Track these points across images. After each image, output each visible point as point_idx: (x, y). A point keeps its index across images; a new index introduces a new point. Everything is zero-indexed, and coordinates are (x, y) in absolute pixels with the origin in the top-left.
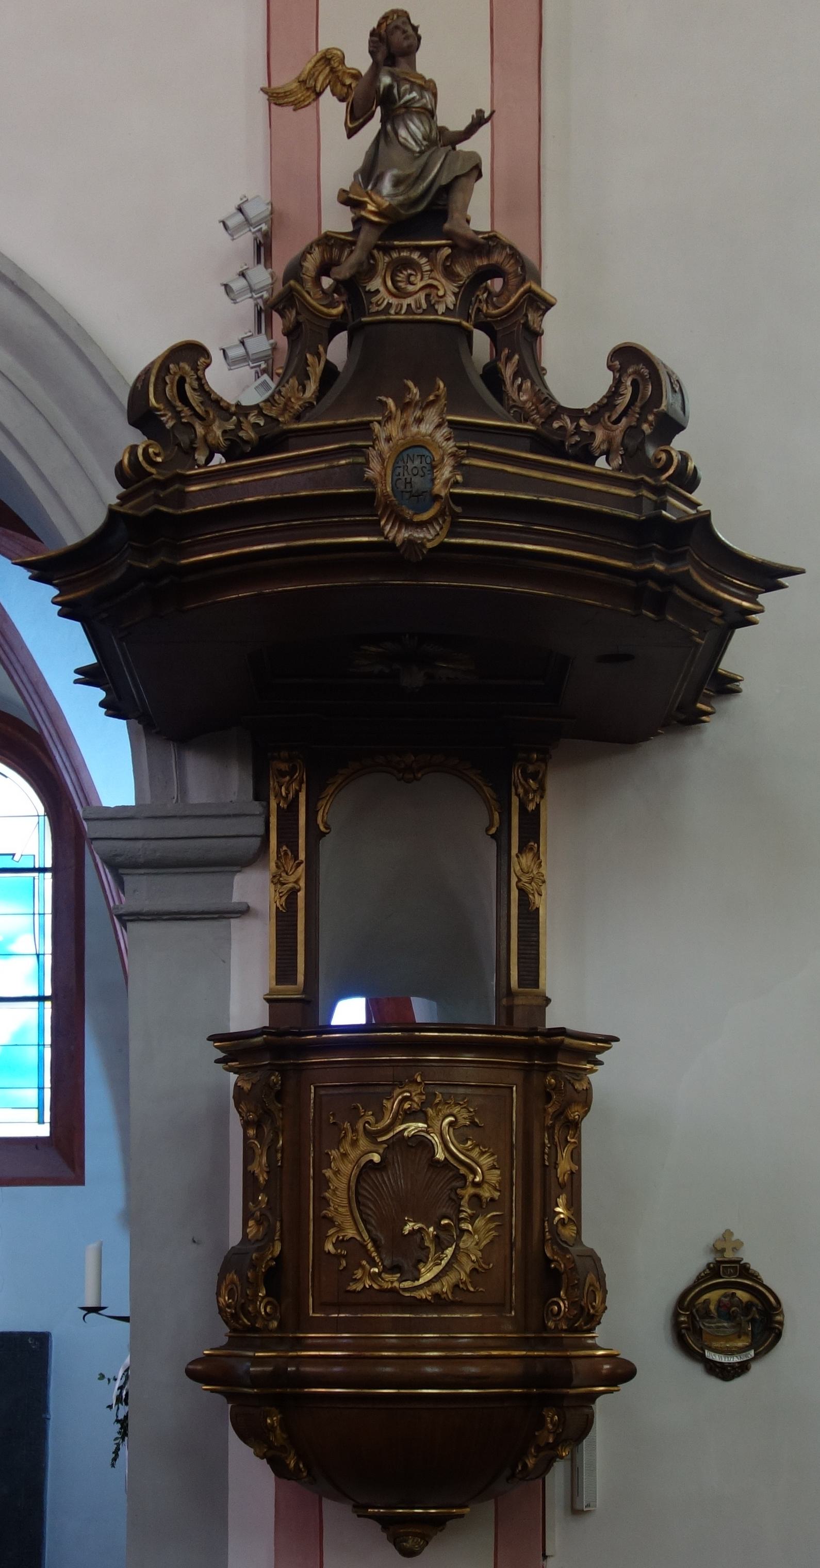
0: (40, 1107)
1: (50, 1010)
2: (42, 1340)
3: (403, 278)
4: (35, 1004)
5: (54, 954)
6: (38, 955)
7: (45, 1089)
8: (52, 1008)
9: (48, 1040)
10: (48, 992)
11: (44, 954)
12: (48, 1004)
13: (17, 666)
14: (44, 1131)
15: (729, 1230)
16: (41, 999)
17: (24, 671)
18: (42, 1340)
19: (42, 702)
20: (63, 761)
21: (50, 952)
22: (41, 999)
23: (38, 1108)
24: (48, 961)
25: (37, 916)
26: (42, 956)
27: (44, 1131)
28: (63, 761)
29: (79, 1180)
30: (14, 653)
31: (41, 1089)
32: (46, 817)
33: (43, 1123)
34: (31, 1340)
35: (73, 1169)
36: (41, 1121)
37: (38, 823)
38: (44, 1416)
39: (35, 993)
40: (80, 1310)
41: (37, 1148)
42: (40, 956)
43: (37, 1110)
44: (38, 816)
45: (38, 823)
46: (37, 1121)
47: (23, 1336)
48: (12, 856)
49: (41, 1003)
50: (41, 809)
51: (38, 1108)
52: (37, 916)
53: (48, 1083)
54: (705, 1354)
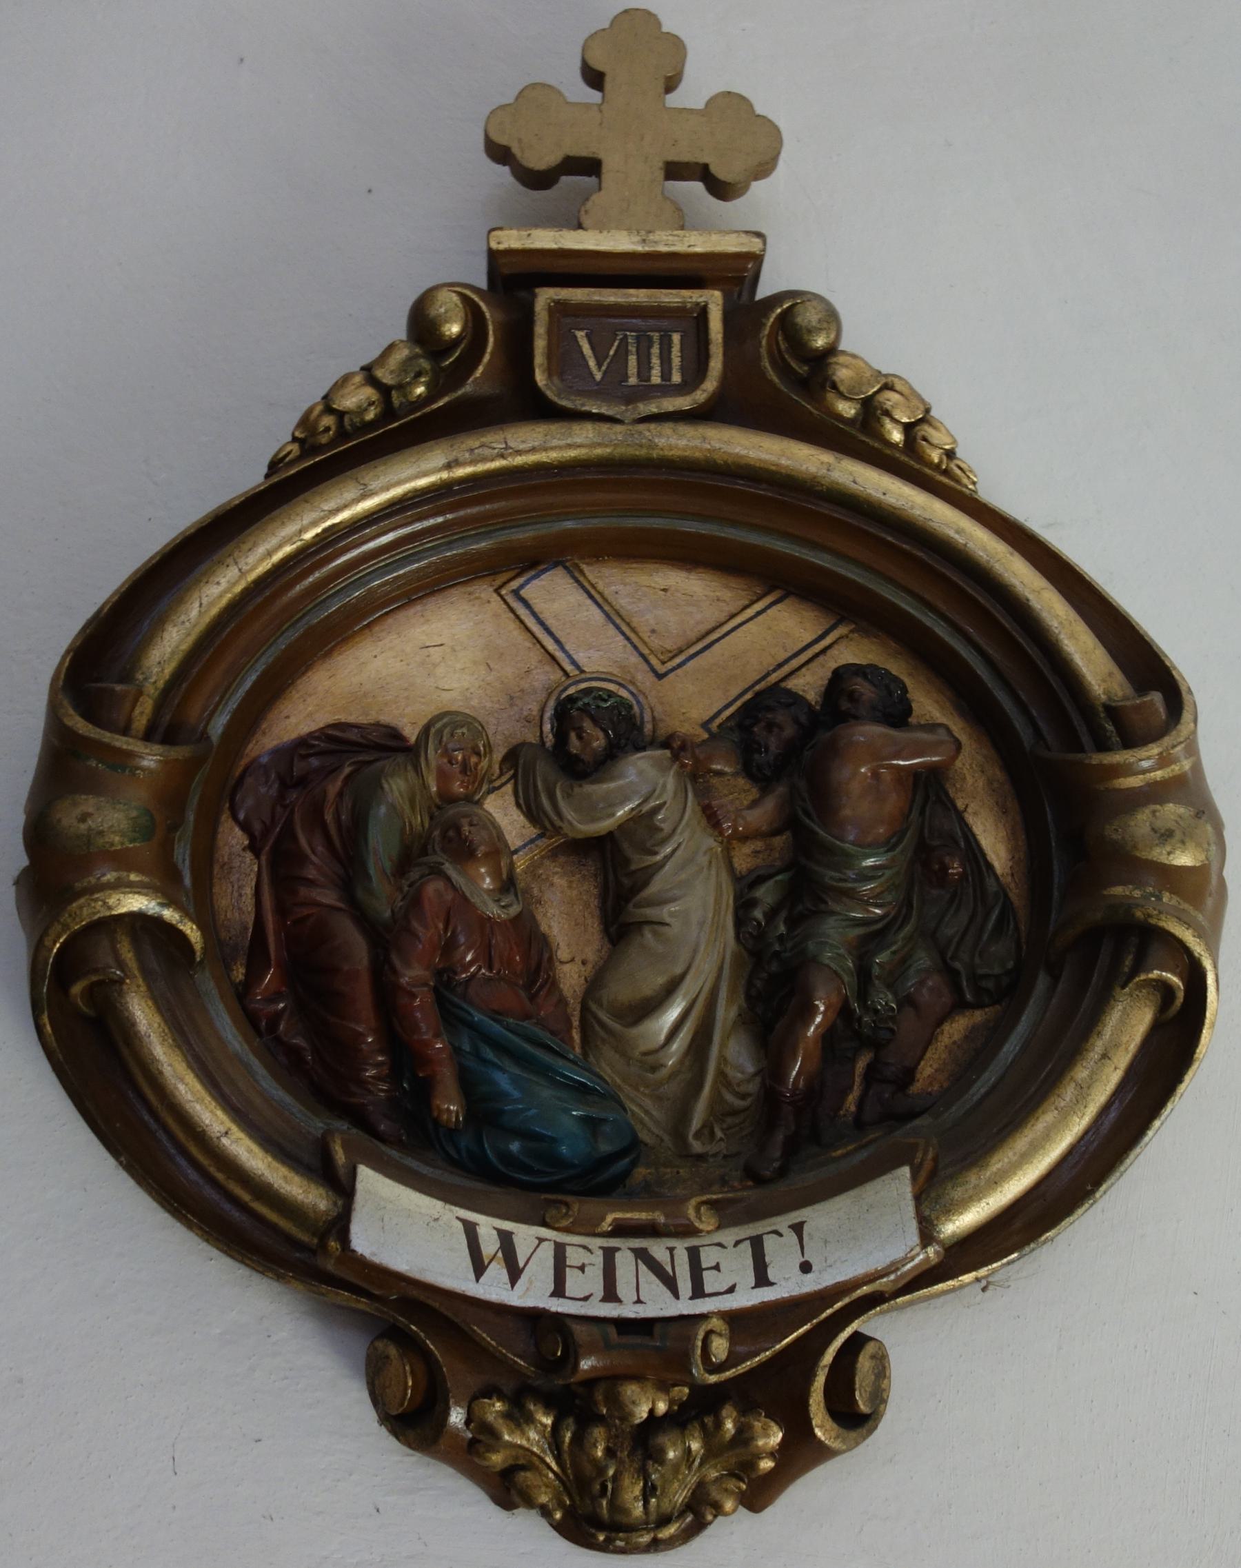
15: (649, 18)
54: (340, 1224)
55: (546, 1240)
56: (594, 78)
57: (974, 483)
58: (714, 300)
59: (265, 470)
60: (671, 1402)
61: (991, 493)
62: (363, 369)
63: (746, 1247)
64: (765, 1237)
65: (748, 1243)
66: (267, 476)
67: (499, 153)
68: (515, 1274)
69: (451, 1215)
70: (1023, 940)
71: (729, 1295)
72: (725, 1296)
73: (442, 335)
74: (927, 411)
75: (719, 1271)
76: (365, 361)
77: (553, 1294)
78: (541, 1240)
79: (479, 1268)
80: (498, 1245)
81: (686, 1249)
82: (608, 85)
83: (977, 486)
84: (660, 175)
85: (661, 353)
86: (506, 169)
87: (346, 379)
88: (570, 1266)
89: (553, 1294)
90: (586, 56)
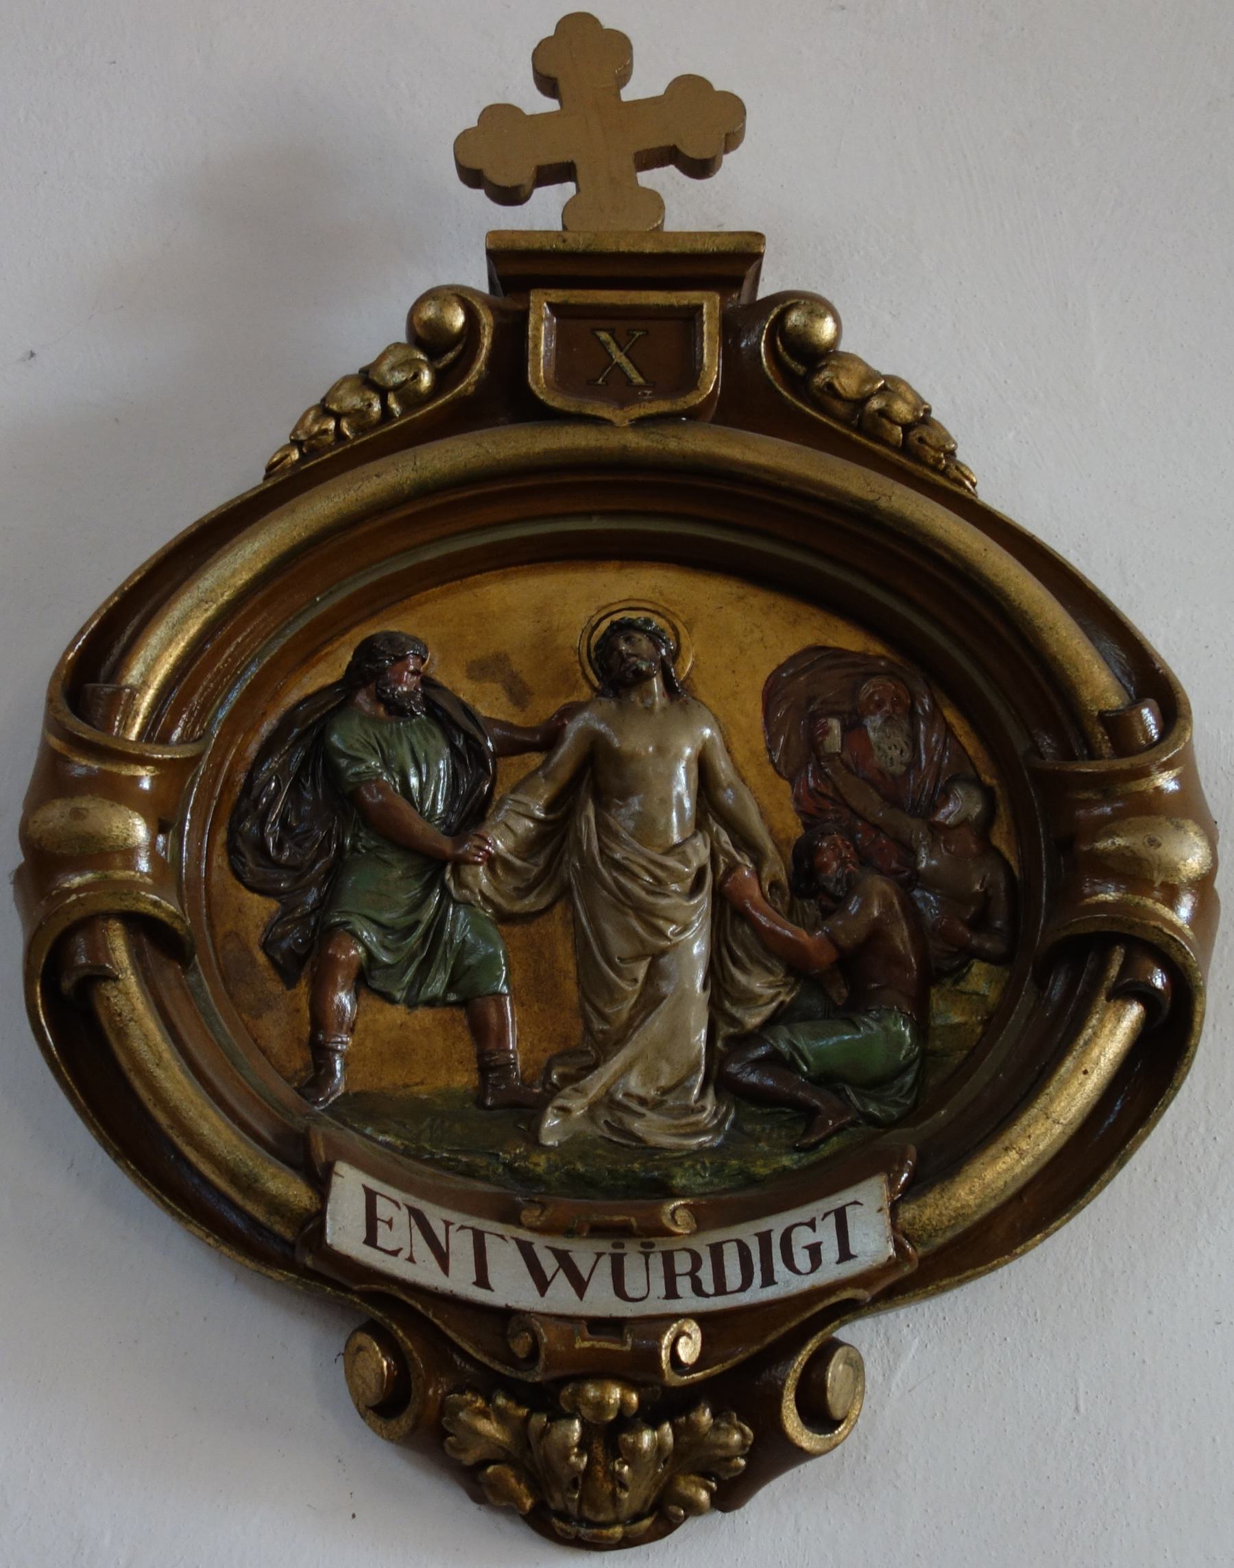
54: (318, 1218)
55: (604, 1253)
56: (547, 84)
57: (974, 485)
58: (710, 304)
59: (263, 473)
60: (604, 1390)
61: (989, 494)
62: (362, 371)
63: (832, 1219)
64: (675, 1253)
65: (833, 1214)
66: (266, 478)
67: (471, 177)
68: (580, 1285)
69: (1116, 975)
70: (676, 1122)
71: (741, 1294)
72: (737, 1294)
73: (422, 394)
74: (928, 411)
75: (814, 1230)
76: (368, 359)
77: (668, 1297)
78: (599, 1255)
79: (542, 1284)
80: (558, 1265)
81: (775, 1283)
82: (563, 86)
83: (977, 487)
84: (629, 162)
85: (270, 1231)
86: (481, 192)
87: (346, 379)
88: (558, 1270)
89: (668, 1297)
90: (538, 68)
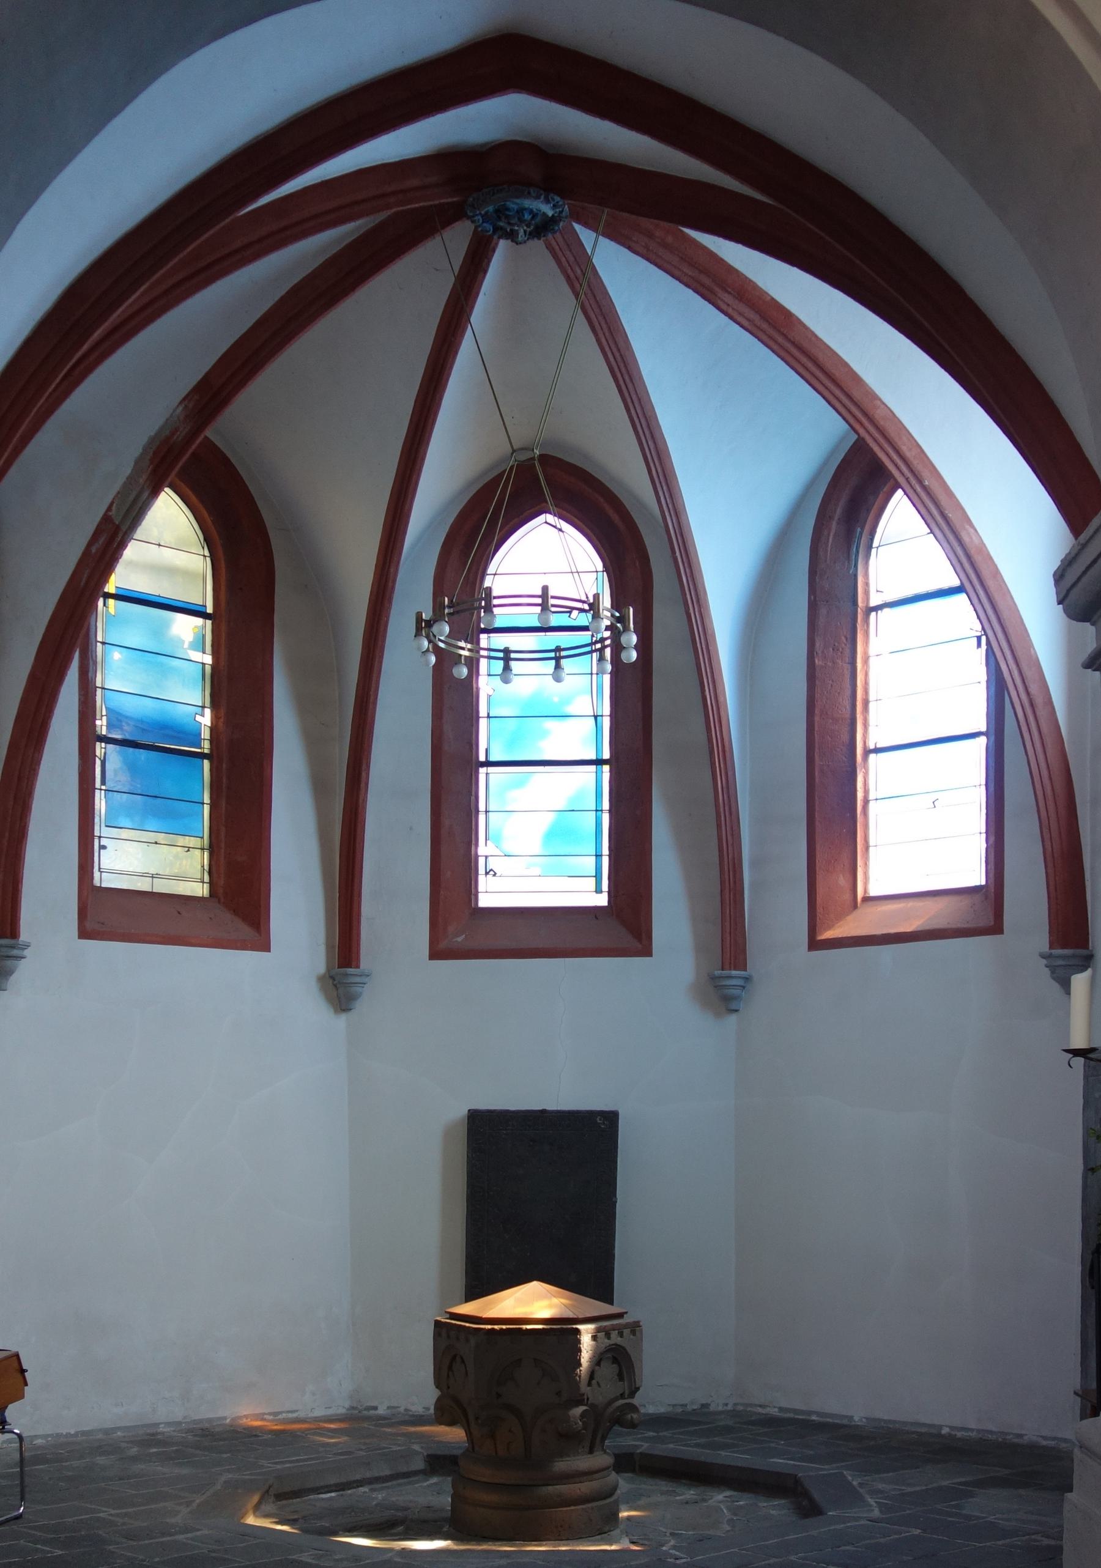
0: (598, 875)
1: (608, 774)
2: (611, 1118)
3: (523, 227)
4: (592, 768)
5: (613, 716)
6: (596, 717)
7: (603, 857)
8: (611, 771)
9: (606, 805)
10: (606, 755)
11: (602, 716)
12: (606, 768)
13: (634, 397)
14: (602, 900)
16: (599, 762)
17: (640, 402)
18: (611, 1118)
19: (653, 437)
20: (666, 502)
21: (608, 713)
22: (599, 762)
23: (595, 876)
24: (606, 723)
25: (594, 676)
26: (601, 717)
27: (602, 900)
28: (666, 502)
29: (647, 951)
30: (633, 384)
31: (598, 856)
32: (605, 573)
33: (601, 892)
34: (600, 1120)
35: (640, 940)
36: (598, 890)
37: (597, 579)
38: (614, 1200)
39: (592, 756)
40: (1062, 1052)
41: (596, 918)
42: (598, 718)
43: (595, 878)
44: (597, 572)
45: (597, 579)
46: (595, 890)
47: (591, 1115)
48: (569, 614)
49: (599, 767)
50: (600, 566)
51: (595, 876)
52: (594, 676)
53: (606, 851)
